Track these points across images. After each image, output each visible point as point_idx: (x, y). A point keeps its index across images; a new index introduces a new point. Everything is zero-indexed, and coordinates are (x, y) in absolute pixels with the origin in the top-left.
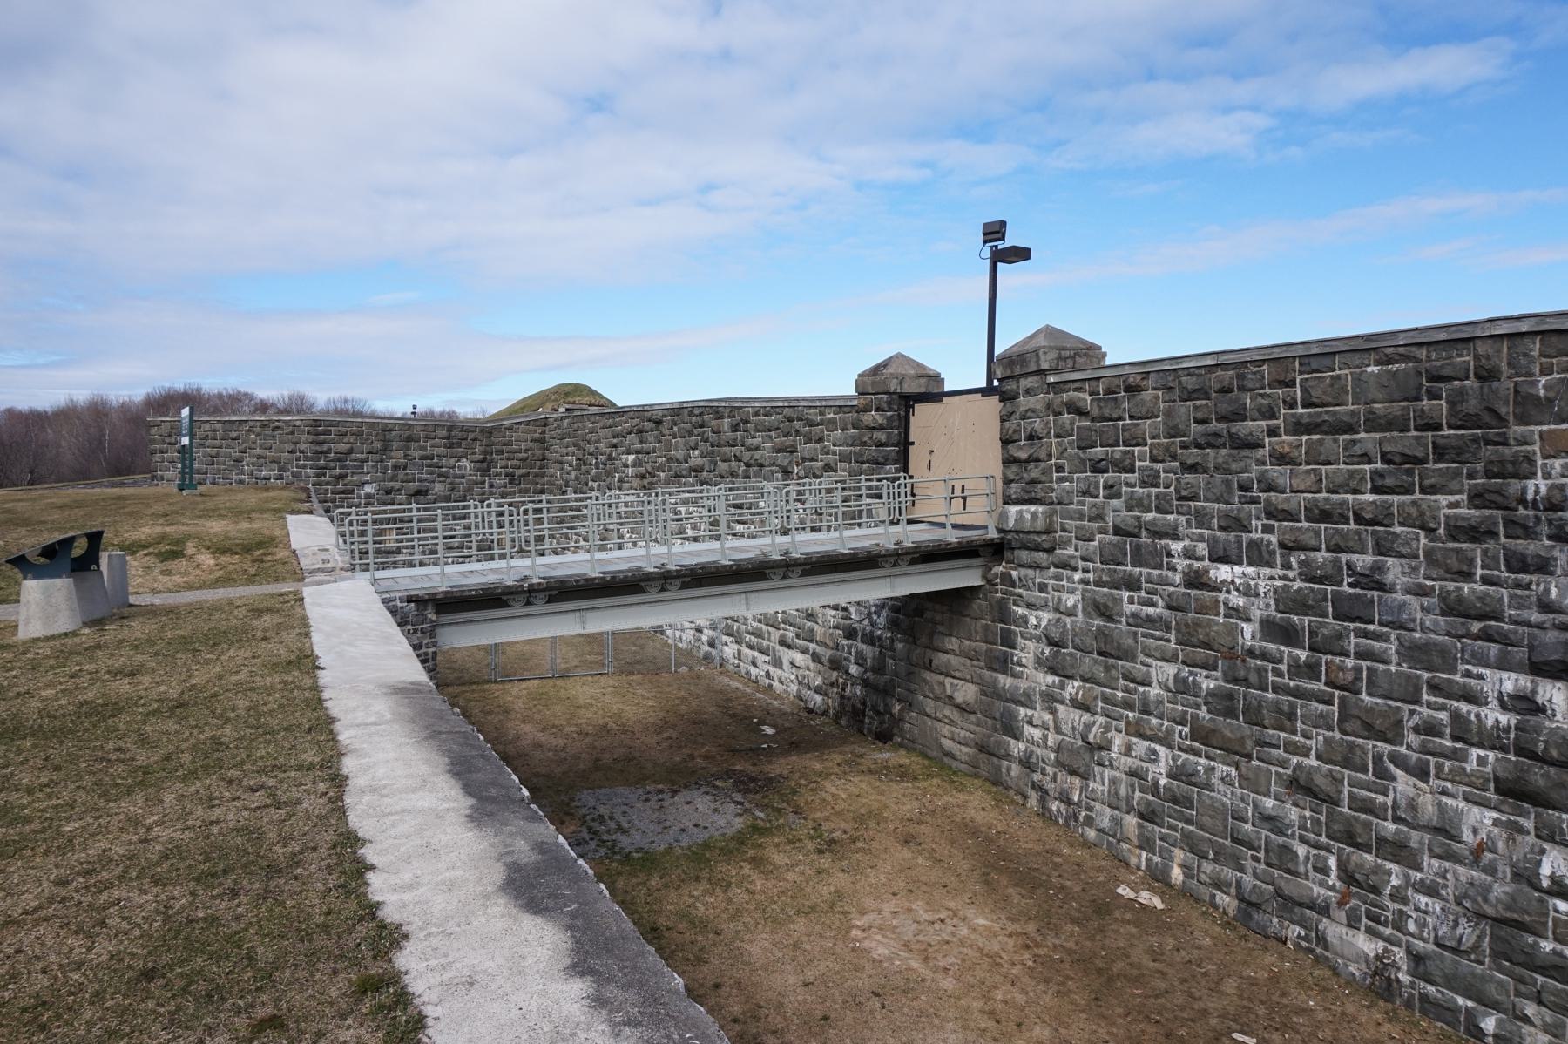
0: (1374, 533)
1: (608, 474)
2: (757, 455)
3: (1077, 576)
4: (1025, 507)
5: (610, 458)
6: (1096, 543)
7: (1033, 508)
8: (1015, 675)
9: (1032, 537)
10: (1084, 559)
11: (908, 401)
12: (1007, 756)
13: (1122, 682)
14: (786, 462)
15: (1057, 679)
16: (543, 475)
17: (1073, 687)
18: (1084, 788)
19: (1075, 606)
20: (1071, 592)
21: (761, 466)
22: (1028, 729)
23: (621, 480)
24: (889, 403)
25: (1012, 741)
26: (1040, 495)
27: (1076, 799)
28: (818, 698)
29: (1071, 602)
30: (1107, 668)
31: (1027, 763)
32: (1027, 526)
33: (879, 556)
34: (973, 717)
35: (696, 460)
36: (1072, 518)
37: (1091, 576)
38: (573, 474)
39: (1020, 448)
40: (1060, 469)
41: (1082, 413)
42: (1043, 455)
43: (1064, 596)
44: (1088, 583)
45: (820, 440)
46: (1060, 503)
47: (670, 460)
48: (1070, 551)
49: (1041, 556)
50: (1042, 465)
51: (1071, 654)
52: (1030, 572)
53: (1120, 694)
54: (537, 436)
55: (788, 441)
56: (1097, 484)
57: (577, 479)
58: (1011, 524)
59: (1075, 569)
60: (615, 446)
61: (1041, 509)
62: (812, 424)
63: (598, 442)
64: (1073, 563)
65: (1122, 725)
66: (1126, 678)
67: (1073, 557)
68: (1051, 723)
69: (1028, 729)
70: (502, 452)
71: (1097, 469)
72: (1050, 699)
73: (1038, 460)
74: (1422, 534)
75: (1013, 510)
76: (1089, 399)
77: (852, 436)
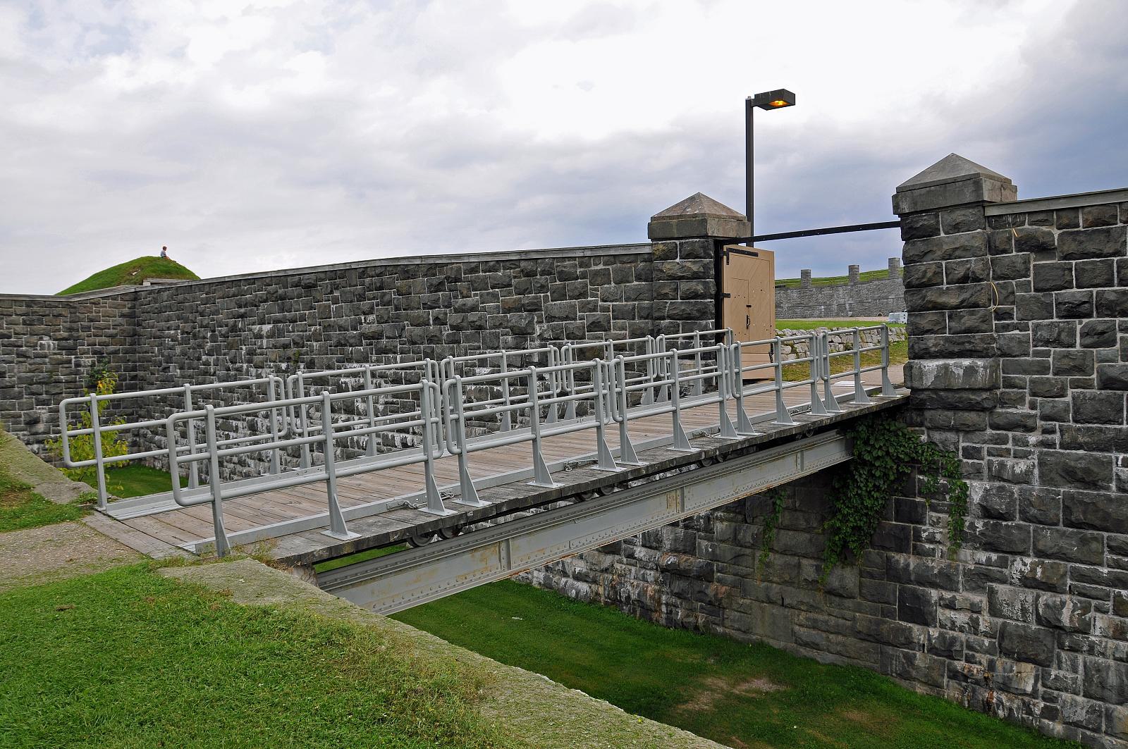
0: (1083, 734)
1: (230, 347)
2: (472, 317)
3: (1033, 438)
4: (951, 362)
5: (234, 329)
6: (1068, 399)
7: (966, 362)
8: (919, 552)
9: (965, 395)
10: (1045, 418)
11: (720, 247)
12: (909, 643)
13: (1107, 556)
14: (523, 323)
15: (994, 556)
16: (134, 352)
17: (1021, 565)
18: (1042, 678)
19: (1028, 473)
20: (1025, 455)
21: (481, 328)
22: (943, 614)
23: (251, 353)
24: (705, 248)
25: (916, 628)
26: (980, 346)
27: (1029, 689)
28: (584, 587)
29: (1021, 466)
30: (1084, 541)
31: (947, 650)
32: (958, 383)
33: (854, 418)
34: (848, 603)
35: (370, 324)
36: (1025, 372)
37: (1057, 437)
38: (178, 350)
39: (942, 292)
40: (1000, 315)
41: (1043, 248)
42: (983, 299)
43: (1009, 462)
44: (1052, 445)
45: (583, 295)
46: (1004, 355)
47: (328, 328)
48: (1025, 410)
49: (972, 417)
50: (982, 311)
51: (1019, 527)
52: (951, 436)
53: (1105, 570)
54: (126, 310)
55: (527, 299)
56: (1072, 333)
57: (184, 354)
58: (928, 381)
59: (1030, 429)
60: (242, 316)
61: (980, 362)
62: (564, 277)
63: (217, 312)
64: (1030, 422)
65: (1109, 604)
66: (1112, 550)
67: (1030, 416)
68: (985, 605)
69: (943, 614)
70: (89, 328)
71: (1073, 311)
72: (980, 578)
73: (976, 305)
74: (667, 573)
75: (931, 365)
76: (1056, 233)
77: (635, 289)
